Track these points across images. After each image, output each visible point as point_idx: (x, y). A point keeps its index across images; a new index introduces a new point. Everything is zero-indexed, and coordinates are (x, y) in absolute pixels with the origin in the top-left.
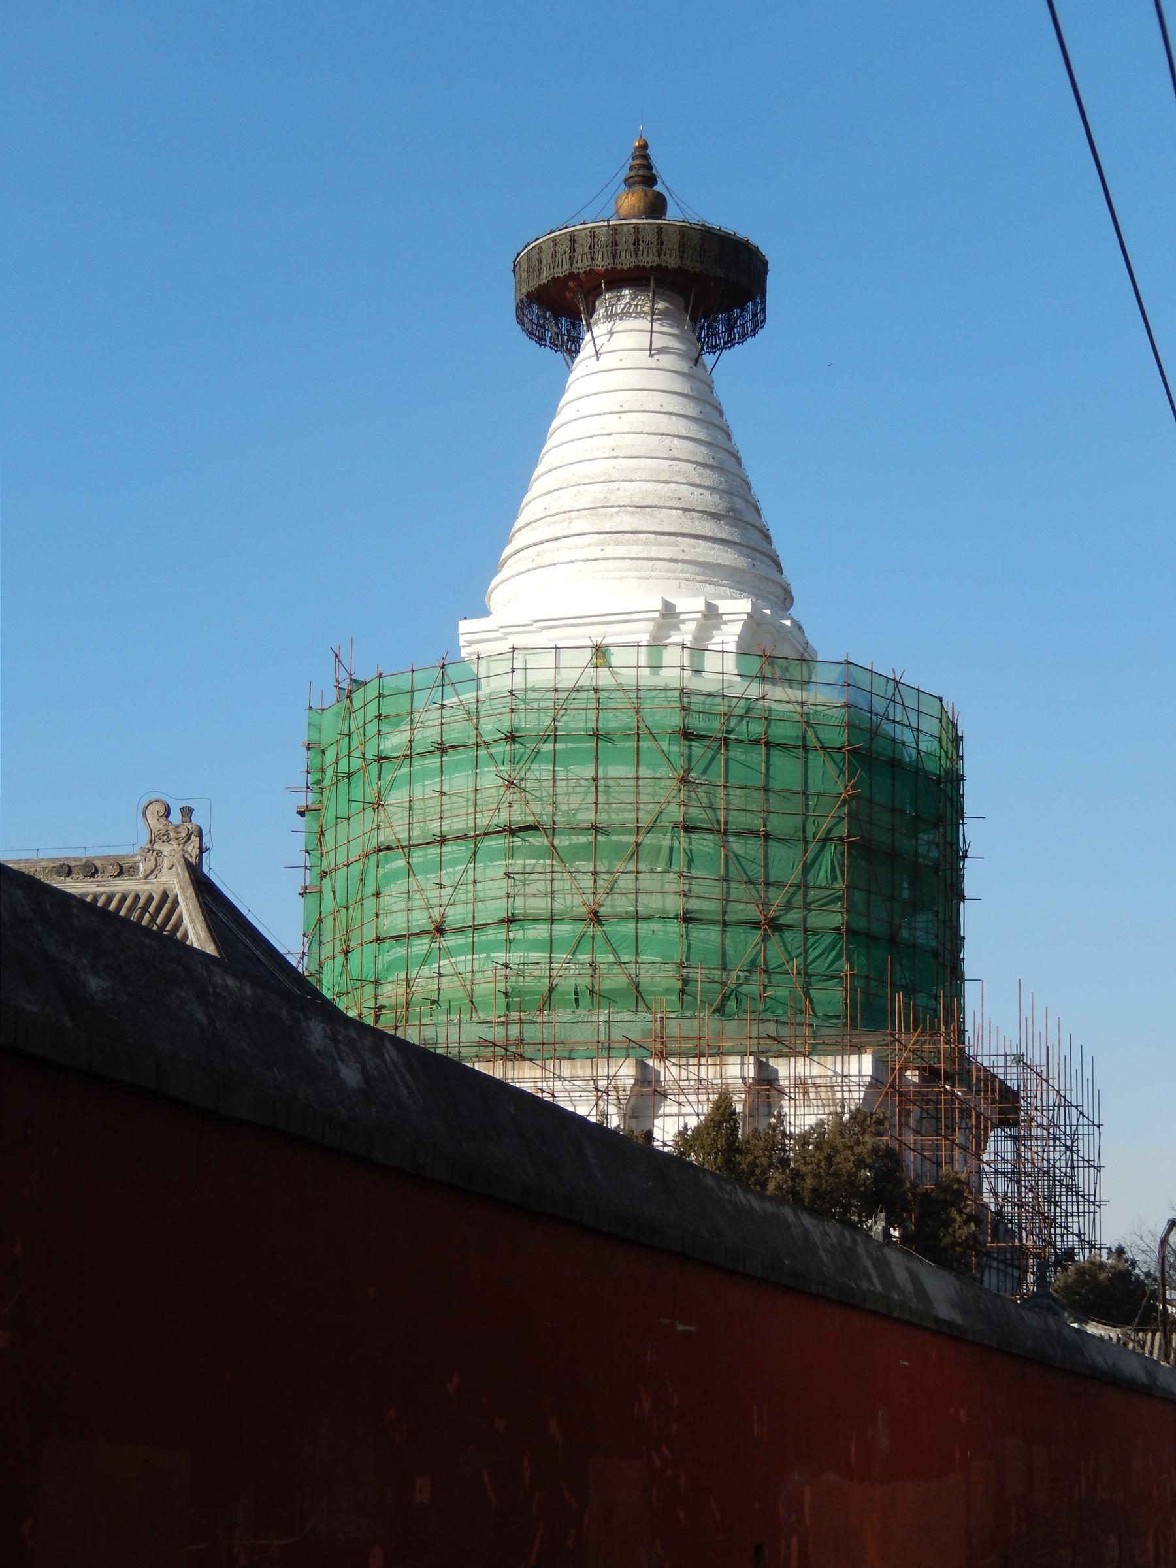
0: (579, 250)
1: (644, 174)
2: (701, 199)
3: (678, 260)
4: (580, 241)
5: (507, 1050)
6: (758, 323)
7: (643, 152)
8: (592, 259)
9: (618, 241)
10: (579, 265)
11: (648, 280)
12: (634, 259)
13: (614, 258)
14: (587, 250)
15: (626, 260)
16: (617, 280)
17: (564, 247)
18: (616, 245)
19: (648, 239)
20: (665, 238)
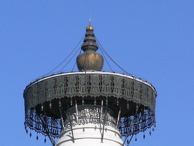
0: (70, 86)
1: (89, 44)
2: (120, 64)
3: (121, 94)
4: (70, 81)
5: (152, 116)
6: (152, 123)
7: (89, 33)
8: (77, 91)
9: (91, 82)
10: (70, 93)
11: (99, 103)
12: (99, 92)
13: (89, 91)
14: (74, 86)
15: (95, 93)
16: (90, 102)
17: (61, 83)
18: (90, 84)
19: (106, 82)
20: (115, 83)
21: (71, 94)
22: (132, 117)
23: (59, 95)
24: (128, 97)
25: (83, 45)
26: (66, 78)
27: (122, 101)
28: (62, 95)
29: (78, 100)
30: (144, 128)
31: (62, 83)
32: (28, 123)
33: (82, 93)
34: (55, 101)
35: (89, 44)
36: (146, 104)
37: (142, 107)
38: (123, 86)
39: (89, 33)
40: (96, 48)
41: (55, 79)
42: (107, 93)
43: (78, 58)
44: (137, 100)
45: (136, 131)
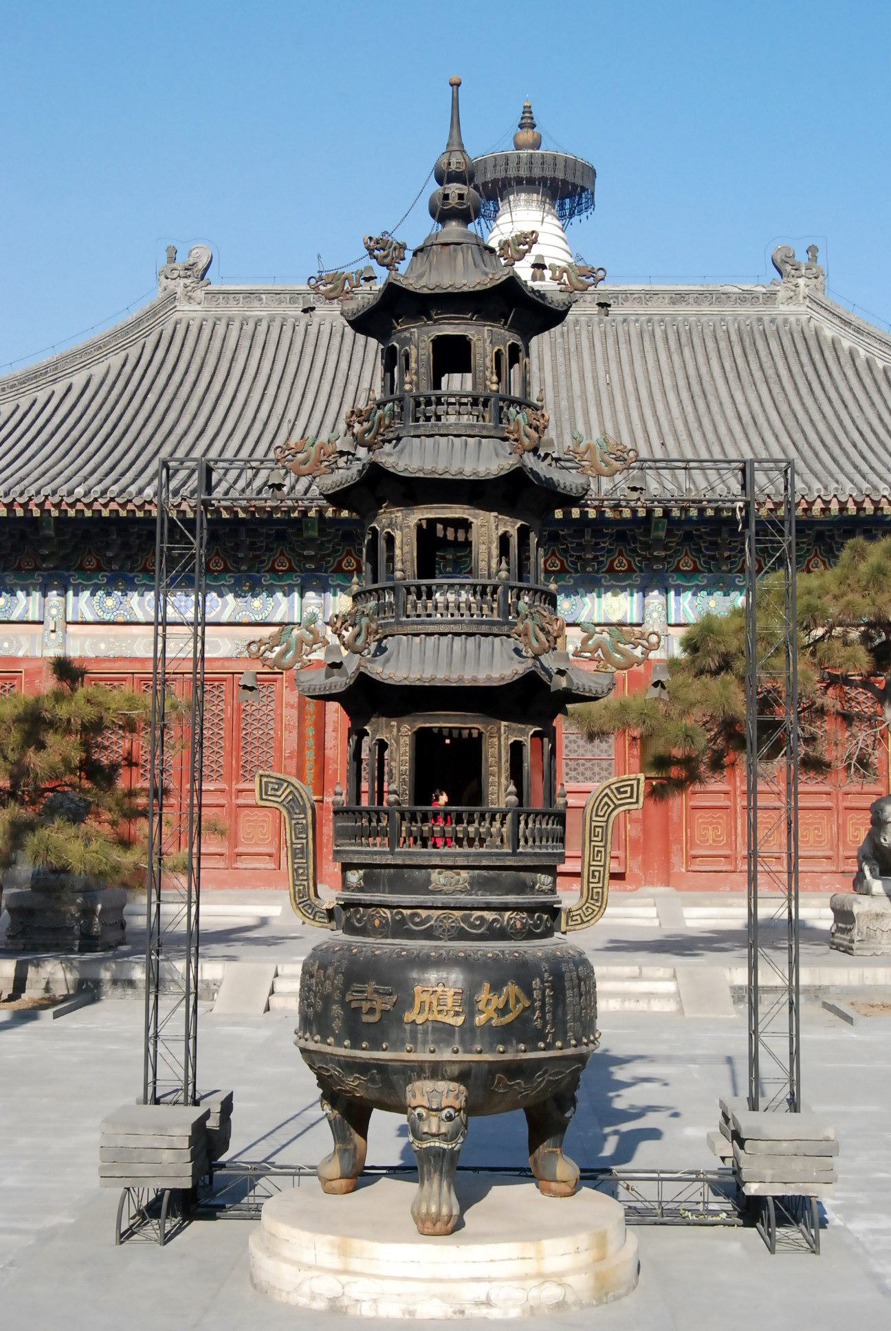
0: (511, 165)
1: (527, 123)
2: (562, 141)
7: (527, 110)
15: (537, 173)
16: (528, 184)
21: (512, 173)
22: (567, 201)
23: (500, 175)
24: (570, 179)
25: (89, 660)
26: (507, 158)
27: (564, 182)
28: (503, 175)
29: (519, 181)
30: (580, 212)
31: (502, 162)
32: (591, 173)
33: (524, 173)
34: (495, 181)
35: (527, 123)
36: (587, 185)
37: (583, 189)
38: (565, 167)
39: (527, 110)
40: (533, 126)
41: (495, 157)
42: (549, 174)
43: (515, 137)
44: (579, 182)
45: (571, 215)
